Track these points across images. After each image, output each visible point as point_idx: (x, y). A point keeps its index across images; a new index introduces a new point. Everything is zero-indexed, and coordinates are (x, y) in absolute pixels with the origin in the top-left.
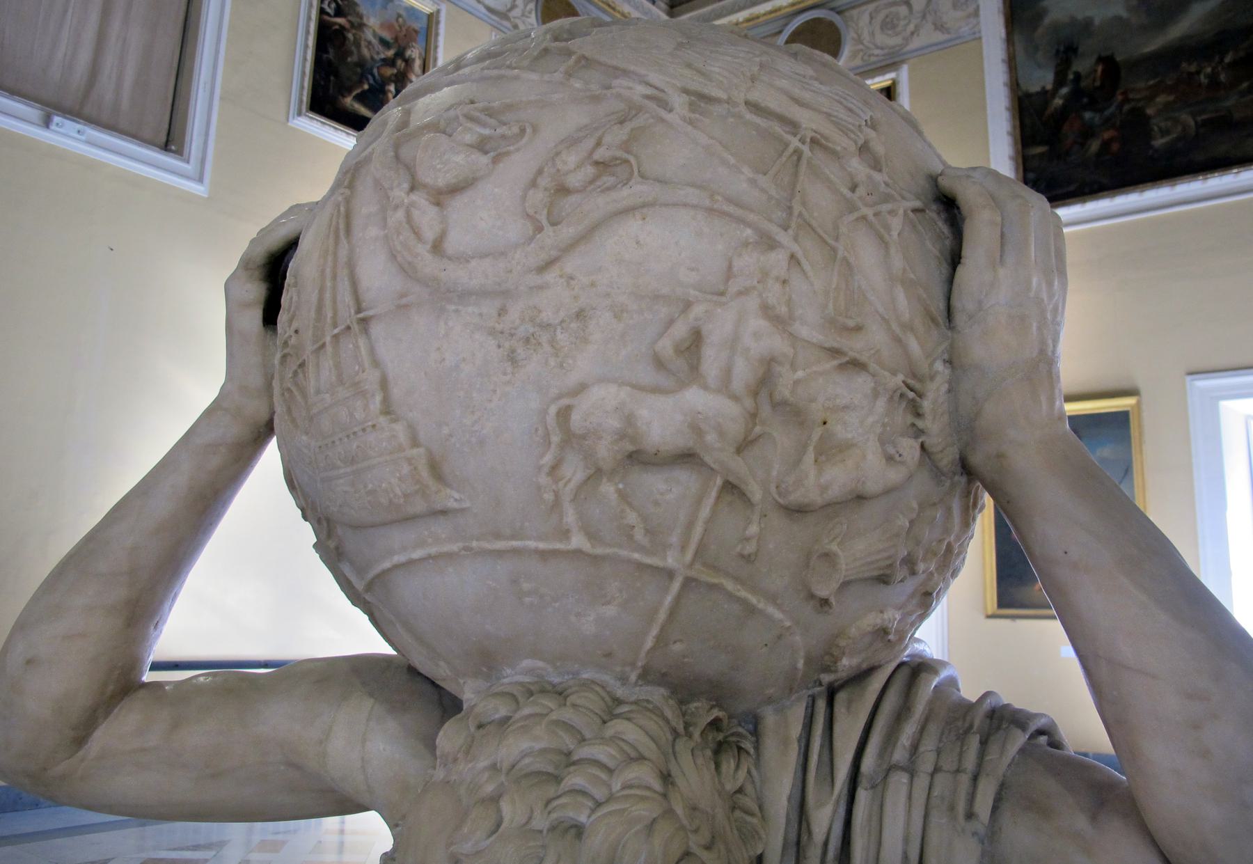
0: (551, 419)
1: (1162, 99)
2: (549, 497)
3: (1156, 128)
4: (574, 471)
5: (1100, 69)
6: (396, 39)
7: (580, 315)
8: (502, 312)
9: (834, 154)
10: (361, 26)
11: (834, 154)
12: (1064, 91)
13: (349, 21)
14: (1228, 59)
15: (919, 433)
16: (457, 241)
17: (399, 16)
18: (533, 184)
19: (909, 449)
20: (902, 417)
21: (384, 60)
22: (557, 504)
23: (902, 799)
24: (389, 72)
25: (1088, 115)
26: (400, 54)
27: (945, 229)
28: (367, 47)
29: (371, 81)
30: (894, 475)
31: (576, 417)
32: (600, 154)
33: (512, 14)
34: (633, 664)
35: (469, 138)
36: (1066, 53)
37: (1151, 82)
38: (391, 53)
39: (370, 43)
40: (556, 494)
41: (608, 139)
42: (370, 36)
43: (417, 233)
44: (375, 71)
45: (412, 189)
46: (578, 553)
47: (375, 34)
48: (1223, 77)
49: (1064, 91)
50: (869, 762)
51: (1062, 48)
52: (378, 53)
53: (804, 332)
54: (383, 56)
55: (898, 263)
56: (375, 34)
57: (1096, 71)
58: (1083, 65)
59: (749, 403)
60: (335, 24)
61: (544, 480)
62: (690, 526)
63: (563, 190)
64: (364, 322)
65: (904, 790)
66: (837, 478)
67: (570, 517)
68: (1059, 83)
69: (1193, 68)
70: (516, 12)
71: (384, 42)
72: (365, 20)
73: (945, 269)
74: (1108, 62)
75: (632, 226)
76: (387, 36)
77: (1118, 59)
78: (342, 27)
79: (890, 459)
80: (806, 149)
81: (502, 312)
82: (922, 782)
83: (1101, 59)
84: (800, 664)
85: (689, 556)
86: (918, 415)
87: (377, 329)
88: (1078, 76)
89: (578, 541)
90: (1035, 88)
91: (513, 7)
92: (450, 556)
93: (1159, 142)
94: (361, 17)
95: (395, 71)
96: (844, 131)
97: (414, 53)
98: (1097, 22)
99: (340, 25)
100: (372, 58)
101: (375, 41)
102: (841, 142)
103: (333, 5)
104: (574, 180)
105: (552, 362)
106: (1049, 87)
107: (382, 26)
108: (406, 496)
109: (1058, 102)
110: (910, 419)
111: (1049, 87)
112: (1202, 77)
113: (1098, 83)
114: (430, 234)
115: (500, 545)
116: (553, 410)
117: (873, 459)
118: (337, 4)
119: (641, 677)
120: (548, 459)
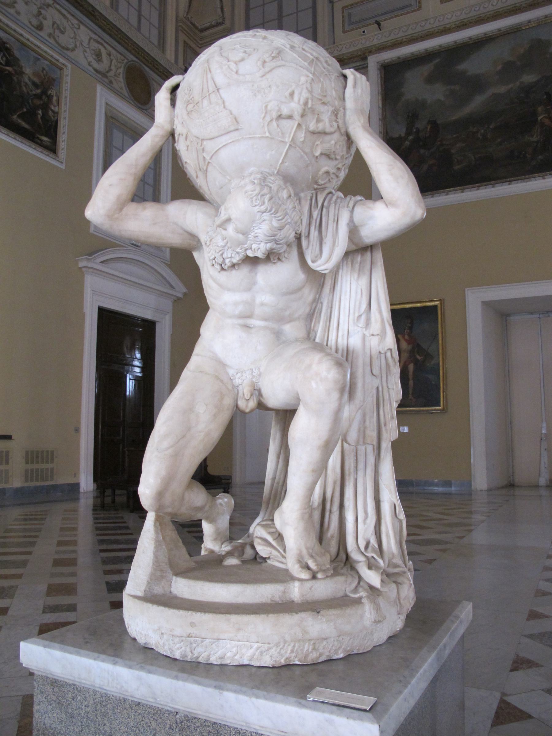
0: (263, 108)
1: (459, 145)
2: (262, 124)
3: (456, 160)
4: (268, 119)
5: (429, 127)
6: (42, 83)
7: (270, 86)
8: (253, 86)
9: (321, 62)
10: (22, 73)
11: (321, 62)
12: (411, 138)
13: (14, 69)
14: (491, 127)
15: (337, 122)
16: (241, 71)
17: (44, 69)
18: (259, 60)
19: (335, 124)
20: (333, 118)
21: (35, 95)
22: (263, 126)
23: (333, 209)
24: (38, 102)
25: (422, 151)
26: (44, 92)
27: (344, 83)
28: (25, 86)
29: (28, 107)
30: (332, 130)
31: (269, 108)
32: (273, 55)
33: (108, 74)
34: (276, 168)
35: (242, 51)
36: (412, 117)
37: (454, 136)
38: (39, 91)
39: (26, 83)
40: (264, 124)
41: (274, 52)
42: (27, 80)
43: (231, 70)
44: (30, 101)
45: (229, 61)
46: (267, 137)
47: (30, 79)
48: (489, 136)
49: (411, 138)
50: (326, 204)
51: (410, 115)
52: (32, 91)
53: (314, 95)
54: (34, 92)
55: (333, 85)
56: (30, 79)
57: (427, 128)
58: (420, 125)
59: (303, 107)
60: (6, 70)
61: (261, 120)
62: (291, 133)
63: (265, 62)
64: (218, 90)
65: (334, 207)
66: (320, 126)
67: (266, 129)
68: (408, 133)
69: (475, 130)
70: (111, 74)
71: (34, 84)
72: (24, 70)
73: (343, 90)
74: (434, 124)
75: (280, 70)
76: (36, 80)
77: (439, 122)
78: (10, 74)
79: (331, 126)
80: (315, 60)
81: (253, 86)
82: (337, 205)
83: (429, 122)
84: (311, 177)
85: (290, 139)
86: (337, 118)
87: (221, 91)
88: (418, 131)
89: (267, 134)
90: (396, 135)
91: (110, 70)
92: (238, 141)
93: (456, 167)
94: (21, 68)
95: (42, 102)
96: (323, 57)
97: (52, 92)
98: (429, 101)
99: (9, 71)
100: (28, 93)
101: (30, 83)
102: (322, 59)
103: (4, 59)
104: (267, 60)
105: (264, 96)
106: (403, 135)
107: (34, 74)
108: (229, 126)
109: (407, 143)
110: (335, 118)
111: (403, 135)
112: (479, 135)
113: (428, 135)
114: (235, 70)
115: (250, 136)
116: (264, 105)
117: (327, 124)
118: (7, 58)
119: (278, 172)
120: (263, 115)
